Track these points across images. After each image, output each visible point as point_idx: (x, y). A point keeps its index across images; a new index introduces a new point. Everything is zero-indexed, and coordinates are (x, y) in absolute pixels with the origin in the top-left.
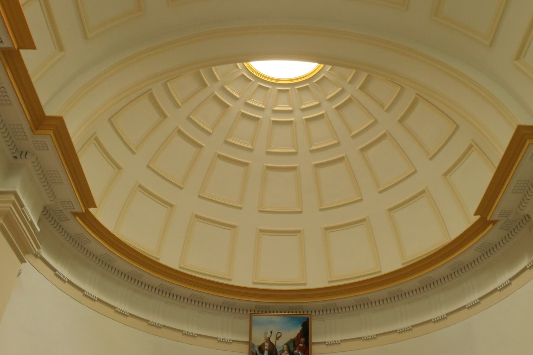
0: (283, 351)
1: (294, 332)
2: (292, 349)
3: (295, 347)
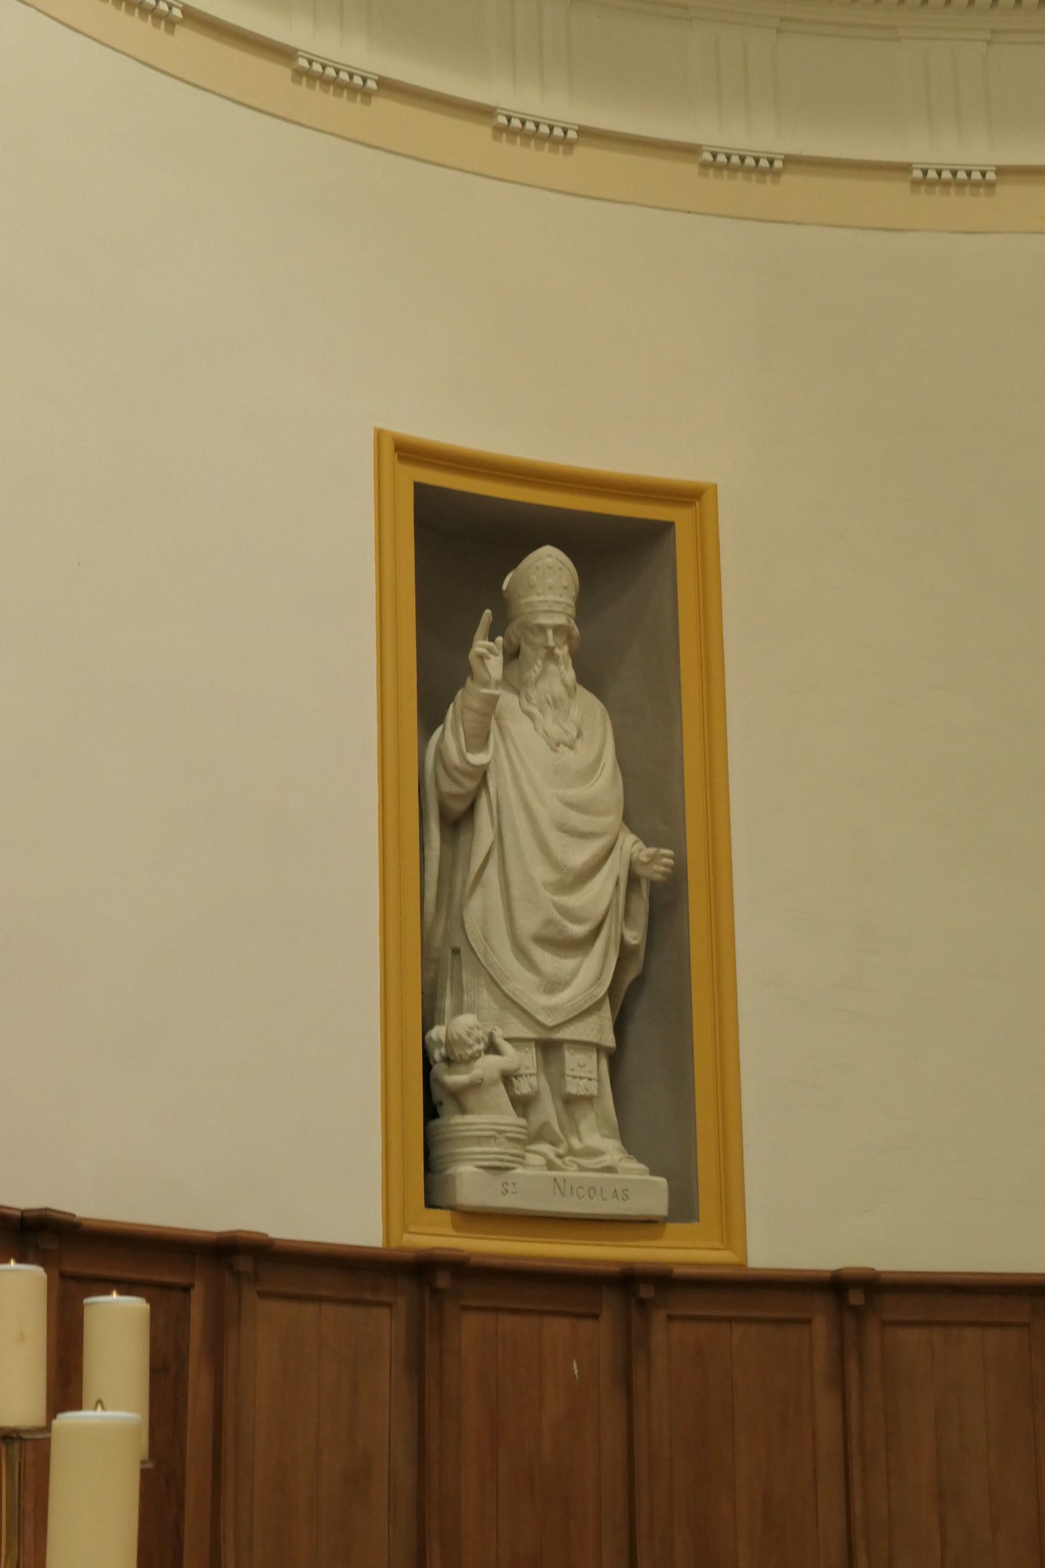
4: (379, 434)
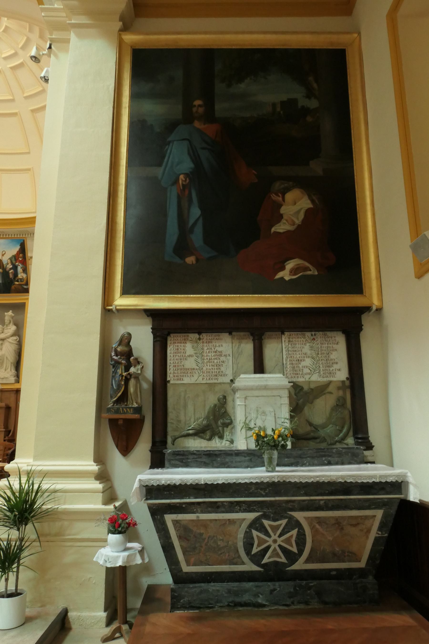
0: (8, 264)
1: (14, 250)
2: (14, 262)
3: (16, 260)
4: (32, 221)
